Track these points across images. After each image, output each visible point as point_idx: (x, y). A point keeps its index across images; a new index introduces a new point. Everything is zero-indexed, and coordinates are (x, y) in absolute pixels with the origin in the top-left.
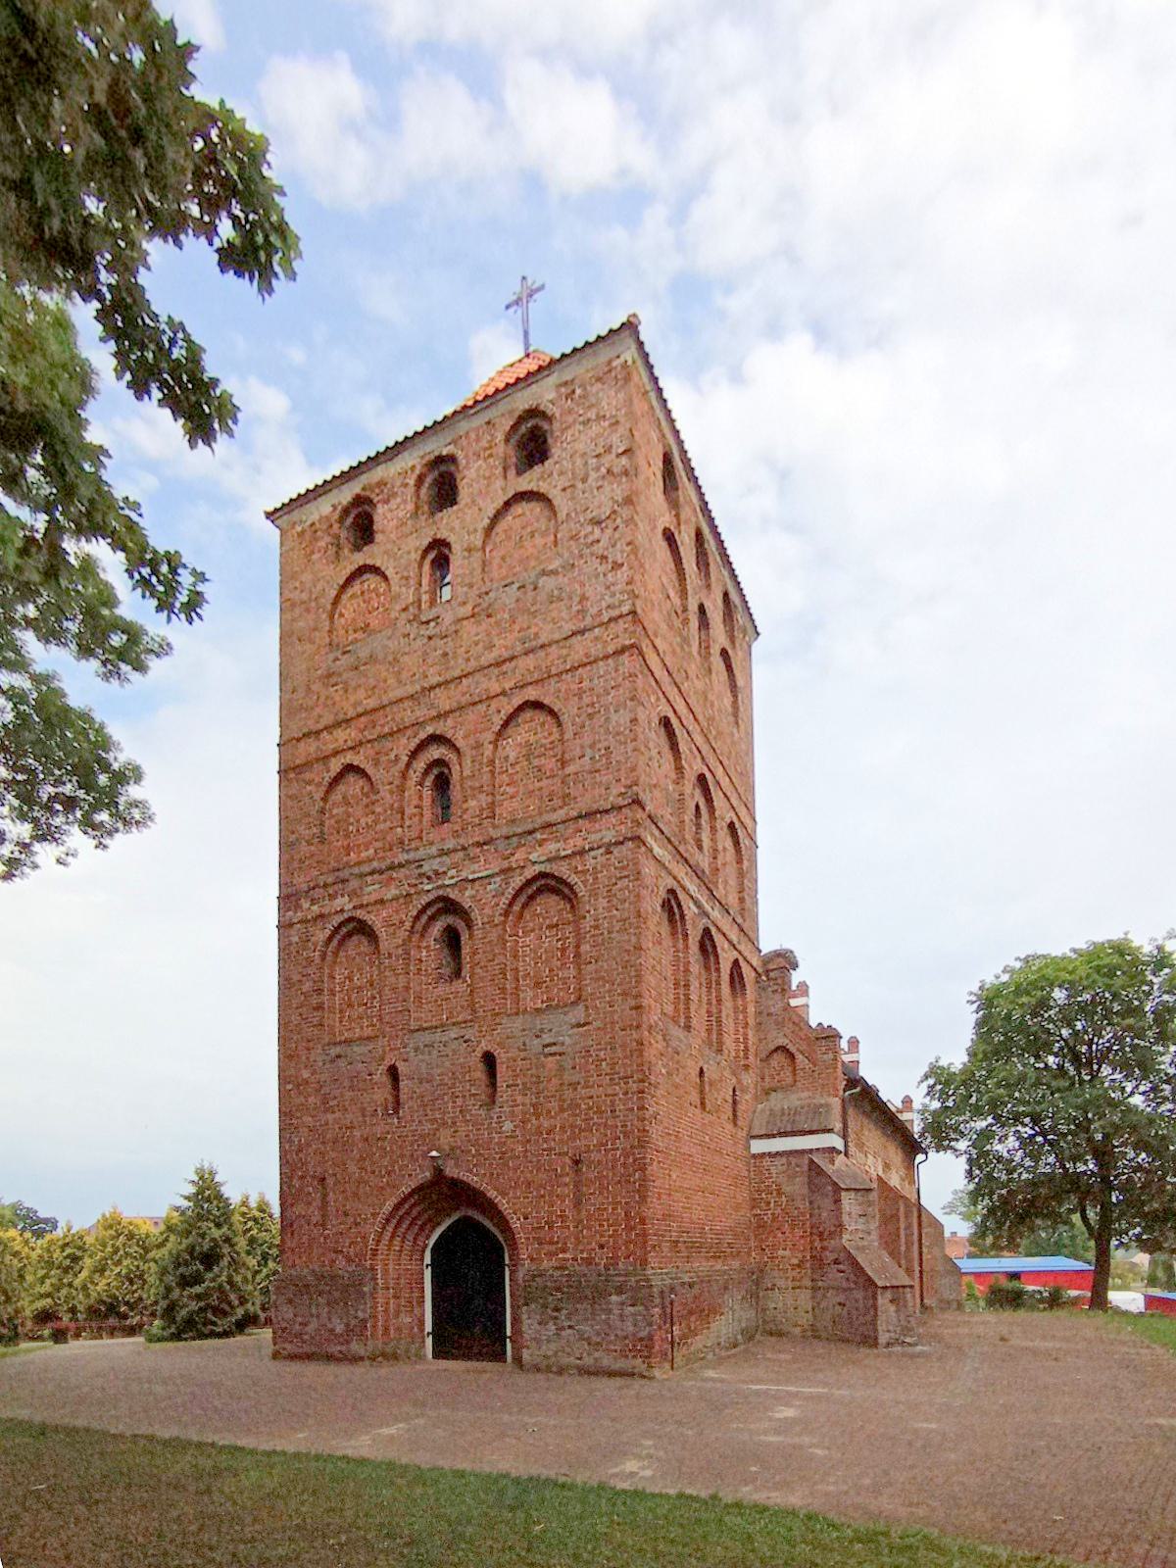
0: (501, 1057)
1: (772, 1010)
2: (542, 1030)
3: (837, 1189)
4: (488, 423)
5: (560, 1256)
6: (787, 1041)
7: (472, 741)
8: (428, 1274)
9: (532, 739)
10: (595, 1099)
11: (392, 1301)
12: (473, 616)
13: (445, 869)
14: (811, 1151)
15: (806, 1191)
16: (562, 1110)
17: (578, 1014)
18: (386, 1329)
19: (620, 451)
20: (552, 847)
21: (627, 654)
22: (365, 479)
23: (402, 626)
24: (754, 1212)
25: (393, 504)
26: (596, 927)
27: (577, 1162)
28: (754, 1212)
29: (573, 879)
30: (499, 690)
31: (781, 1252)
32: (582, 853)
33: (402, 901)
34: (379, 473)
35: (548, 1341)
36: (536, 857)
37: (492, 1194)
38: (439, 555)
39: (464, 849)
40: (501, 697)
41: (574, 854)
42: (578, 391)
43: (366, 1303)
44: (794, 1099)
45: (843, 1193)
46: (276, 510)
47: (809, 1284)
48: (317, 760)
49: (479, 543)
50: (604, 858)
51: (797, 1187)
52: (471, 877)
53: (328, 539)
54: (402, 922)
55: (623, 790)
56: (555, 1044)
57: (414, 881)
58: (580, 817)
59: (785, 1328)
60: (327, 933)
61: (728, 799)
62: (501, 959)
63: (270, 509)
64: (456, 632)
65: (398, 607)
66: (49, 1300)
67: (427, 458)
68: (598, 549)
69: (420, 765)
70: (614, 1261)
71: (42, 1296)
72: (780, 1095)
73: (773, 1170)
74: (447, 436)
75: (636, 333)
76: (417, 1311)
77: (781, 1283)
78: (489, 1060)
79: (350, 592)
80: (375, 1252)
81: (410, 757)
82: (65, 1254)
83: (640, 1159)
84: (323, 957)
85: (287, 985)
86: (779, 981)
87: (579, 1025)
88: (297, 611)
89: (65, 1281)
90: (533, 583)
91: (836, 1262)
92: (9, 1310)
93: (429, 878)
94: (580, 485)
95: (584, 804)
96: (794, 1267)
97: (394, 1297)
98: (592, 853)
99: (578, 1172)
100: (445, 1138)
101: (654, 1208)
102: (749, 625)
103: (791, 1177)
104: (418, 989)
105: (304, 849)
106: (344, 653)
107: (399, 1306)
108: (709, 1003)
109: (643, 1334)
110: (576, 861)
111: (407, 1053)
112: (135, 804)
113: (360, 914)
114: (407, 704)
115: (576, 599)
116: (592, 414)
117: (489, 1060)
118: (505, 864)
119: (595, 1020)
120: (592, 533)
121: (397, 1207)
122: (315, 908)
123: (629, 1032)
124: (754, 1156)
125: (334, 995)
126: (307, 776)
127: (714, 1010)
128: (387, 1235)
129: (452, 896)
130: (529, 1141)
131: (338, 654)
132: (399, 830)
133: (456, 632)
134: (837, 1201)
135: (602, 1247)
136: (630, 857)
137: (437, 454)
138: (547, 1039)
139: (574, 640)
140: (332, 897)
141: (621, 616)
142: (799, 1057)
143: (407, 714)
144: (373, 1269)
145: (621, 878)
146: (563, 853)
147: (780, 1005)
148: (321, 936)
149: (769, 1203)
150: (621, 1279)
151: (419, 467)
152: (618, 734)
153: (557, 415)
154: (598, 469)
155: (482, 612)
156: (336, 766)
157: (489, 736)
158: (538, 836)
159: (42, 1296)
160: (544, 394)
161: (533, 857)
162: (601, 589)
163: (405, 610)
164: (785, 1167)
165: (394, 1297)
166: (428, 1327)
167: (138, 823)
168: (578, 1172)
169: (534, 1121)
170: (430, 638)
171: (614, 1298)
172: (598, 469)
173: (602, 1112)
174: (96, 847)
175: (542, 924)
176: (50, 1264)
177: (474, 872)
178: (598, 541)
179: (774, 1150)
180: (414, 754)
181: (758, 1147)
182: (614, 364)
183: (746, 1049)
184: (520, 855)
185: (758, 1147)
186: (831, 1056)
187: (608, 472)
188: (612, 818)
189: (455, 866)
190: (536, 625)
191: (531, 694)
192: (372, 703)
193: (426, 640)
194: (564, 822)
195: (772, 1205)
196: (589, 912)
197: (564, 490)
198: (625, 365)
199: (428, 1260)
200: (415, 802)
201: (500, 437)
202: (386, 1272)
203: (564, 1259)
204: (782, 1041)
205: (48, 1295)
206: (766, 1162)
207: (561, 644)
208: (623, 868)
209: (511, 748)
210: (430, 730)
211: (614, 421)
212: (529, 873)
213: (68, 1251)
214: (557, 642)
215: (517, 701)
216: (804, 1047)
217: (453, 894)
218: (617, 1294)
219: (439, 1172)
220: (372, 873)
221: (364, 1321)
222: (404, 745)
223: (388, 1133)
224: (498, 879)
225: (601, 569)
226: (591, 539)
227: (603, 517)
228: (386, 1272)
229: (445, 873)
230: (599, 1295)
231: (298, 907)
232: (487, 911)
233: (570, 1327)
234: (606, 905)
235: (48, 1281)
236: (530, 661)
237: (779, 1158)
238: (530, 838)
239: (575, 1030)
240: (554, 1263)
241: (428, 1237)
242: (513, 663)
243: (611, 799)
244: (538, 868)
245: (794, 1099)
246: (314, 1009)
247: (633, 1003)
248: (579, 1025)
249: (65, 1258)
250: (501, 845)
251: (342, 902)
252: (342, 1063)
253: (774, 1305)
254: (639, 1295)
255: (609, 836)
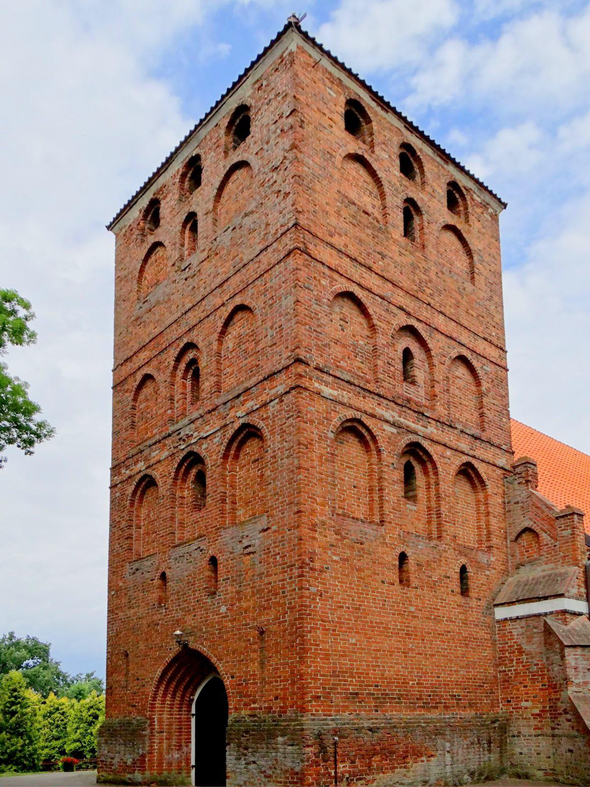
0: (221, 559)
1: (519, 499)
2: (242, 537)
3: (563, 647)
4: (217, 125)
5: (252, 706)
6: (532, 523)
7: (206, 342)
8: (193, 720)
9: (242, 331)
10: (273, 584)
11: (165, 741)
12: (208, 257)
13: (192, 433)
14: (546, 614)
15: (543, 649)
16: (253, 594)
17: (263, 522)
18: (160, 764)
19: (288, 113)
20: (249, 404)
21: (292, 255)
22: (154, 188)
23: (174, 276)
24: (500, 669)
25: (168, 199)
26: (274, 457)
27: (262, 633)
28: (500, 669)
29: (261, 424)
30: (220, 303)
31: (524, 704)
32: (265, 405)
33: (170, 458)
34: (161, 180)
35: (241, 773)
36: (238, 415)
37: (214, 660)
38: (191, 220)
39: (202, 417)
40: (222, 308)
41: (261, 407)
42: (264, 83)
43: (144, 743)
44: (538, 571)
45: (567, 650)
46: (111, 224)
47: (549, 732)
48: (130, 375)
49: (211, 207)
50: (278, 406)
51: (534, 647)
52: (205, 436)
53: (137, 232)
54: (170, 473)
55: (289, 354)
56: (250, 546)
57: (176, 445)
58: (265, 379)
59: (532, 771)
60: (133, 487)
61: (447, 336)
62: (222, 489)
63: (108, 224)
64: (199, 271)
65: (170, 264)
66: (78, 744)
67: (185, 162)
68: (276, 188)
69: (182, 366)
70: (283, 710)
71: (75, 741)
72: (528, 567)
73: (515, 633)
74: (194, 143)
75: (299, 28)
76: (185, 749)
77: (525, 731)
78: (213, 561)
79: (150, 262)
80: (153, 706)
81: (175, 361)
82: (89, 713)
83: (300, 628)
84: (132, 505)
85: (114, 524)
86: (523, 475)
87: (264, 530)
88: (123, 283)
89: (89, 731)
90: (240, 224)
91: (565, 712)
92: (30, 749)
93: (184, 440)
94: (265, 147)
95: (268, 369)
96: (535, 716)
97: (166, 739)
98: (272, 404)
99: (262, 640)
100: (190, 621)
101: (314, 665)
102: (487, 198)
103: (530, 639)
104: (180, 517)
105: (124, 435)
106: (144, 303)
107: (169, 746)
108: (429, 500)
109: (297, 769)
110: (262, 412)
111: (171, 562)
112: (40, 425)
113: (149, 471)
114: (175, 326)
115: (263, 226)
116: (272, 96)
117: (213, 561)
118: (223, 423)
119: (273, 525)
120: (272, 177)
121: (164, 673)
122: (128, 472)
123: (293, 531)
124: (498, 622)
125: (140, 528)
126: (126, 387)
127: (433, 504)
128: (161, 692)
129: (195, 450)
130: (235, 619)
131: (141, 304)
132: (169, 412)
133: (199, 271)
134: (563, 657)
135: (276, 698)
136: (294, 401)
137: (190, 157)
138: (246, 543)
139: (261, 256)
140: (136, 463)
141: (288, 230)
142: (544, 536)
143: (173, 335)
144: (152, 719)
145: (288, 418)
146: (255, 408)
147: (524, 494)
148: (130, 489)
149: (512, 660)
150: (285, 724)
151: (181, 169)
152: (287, 315)
153: (253, 105)
154: (275, 132)
155: (214, 253)
156: (139, 377)
157: (216, 336)
158: (242, 398)
159: (75, 741)
160: (245, 94)
161: (239, 414)
162: (276, 214)
163: (173, 265)
164: (524, 630)
165: (166, 739)
166: (193, 763)
167: (45, 436)
168: (262, 640)
169: (238, 604)
170: (186, 279)
171: (280, 739)
172: (275, 132)
173: (277, 594)
174: (26, 454)
175: (250, 460)
176: (81, 719)
177: (207, 431)
178: (275, 182)
179: (514, 615)
180: (178, 359)
181: (501, 613)
182: (284, 55)
183: (489, 533)
184: (232, 414)
185: (501, 613)
186: (569, 531)
187: (282, 131)
188: (283, 376)
189: (197, 429)
190: (242, 252)
191: (238, 301)
192: (157, 331)
193: (184, 281)
194: (255, 385)
195: (514, 662)
196: (270, 446)
197: (257, 154)
198: (291, 54)
199: (193, 711)
200: (180, 391)
201: (222, 131)
202: (160, 721)
203: (255, 709)
204: (527, 524)
205: (78, 740)
206: (509, 626)
207: (255, 261)
208: (289, 411)
209: (230, 342)
210: (185, 341)
211: (284, 94)
212: (236, 426)
213: (92, 711)
214: (252, 260)
215: (230, 308)
216: (546, 527)
217: (196, 449)
218: (282, 736)
219: (185, 647)
220: (155, 443)
221: (143, 756)
222: (174, 352)
223: (160, 620)
224: (219, 434)
225: (277, 201)
226: (272, 181)
227: (278, 164)
228: (160, 721)
229: (192, 435)
230: (272, 735)
231: (120, 473)
232: (214, 457)
233: (254, 762)
234: (280, 439)
235: (79, 731)
236: (237, 278)
237: (518, 621)
238: (237, 401)
239: (262, 534)
240: (248, 712)
241: (193, 694)
242: (228, 283)
243: (283, 362)
244: (241, 421)
245: (538, 571)
246: (127, 539)
247: (296, 509)
248: (264, 530)
249: (90, 716)
250: (221, 409)
251: (141, 466)
252: (138, 573)
253: (519, 750)
254: (297, 738)
255: (281, 389)
